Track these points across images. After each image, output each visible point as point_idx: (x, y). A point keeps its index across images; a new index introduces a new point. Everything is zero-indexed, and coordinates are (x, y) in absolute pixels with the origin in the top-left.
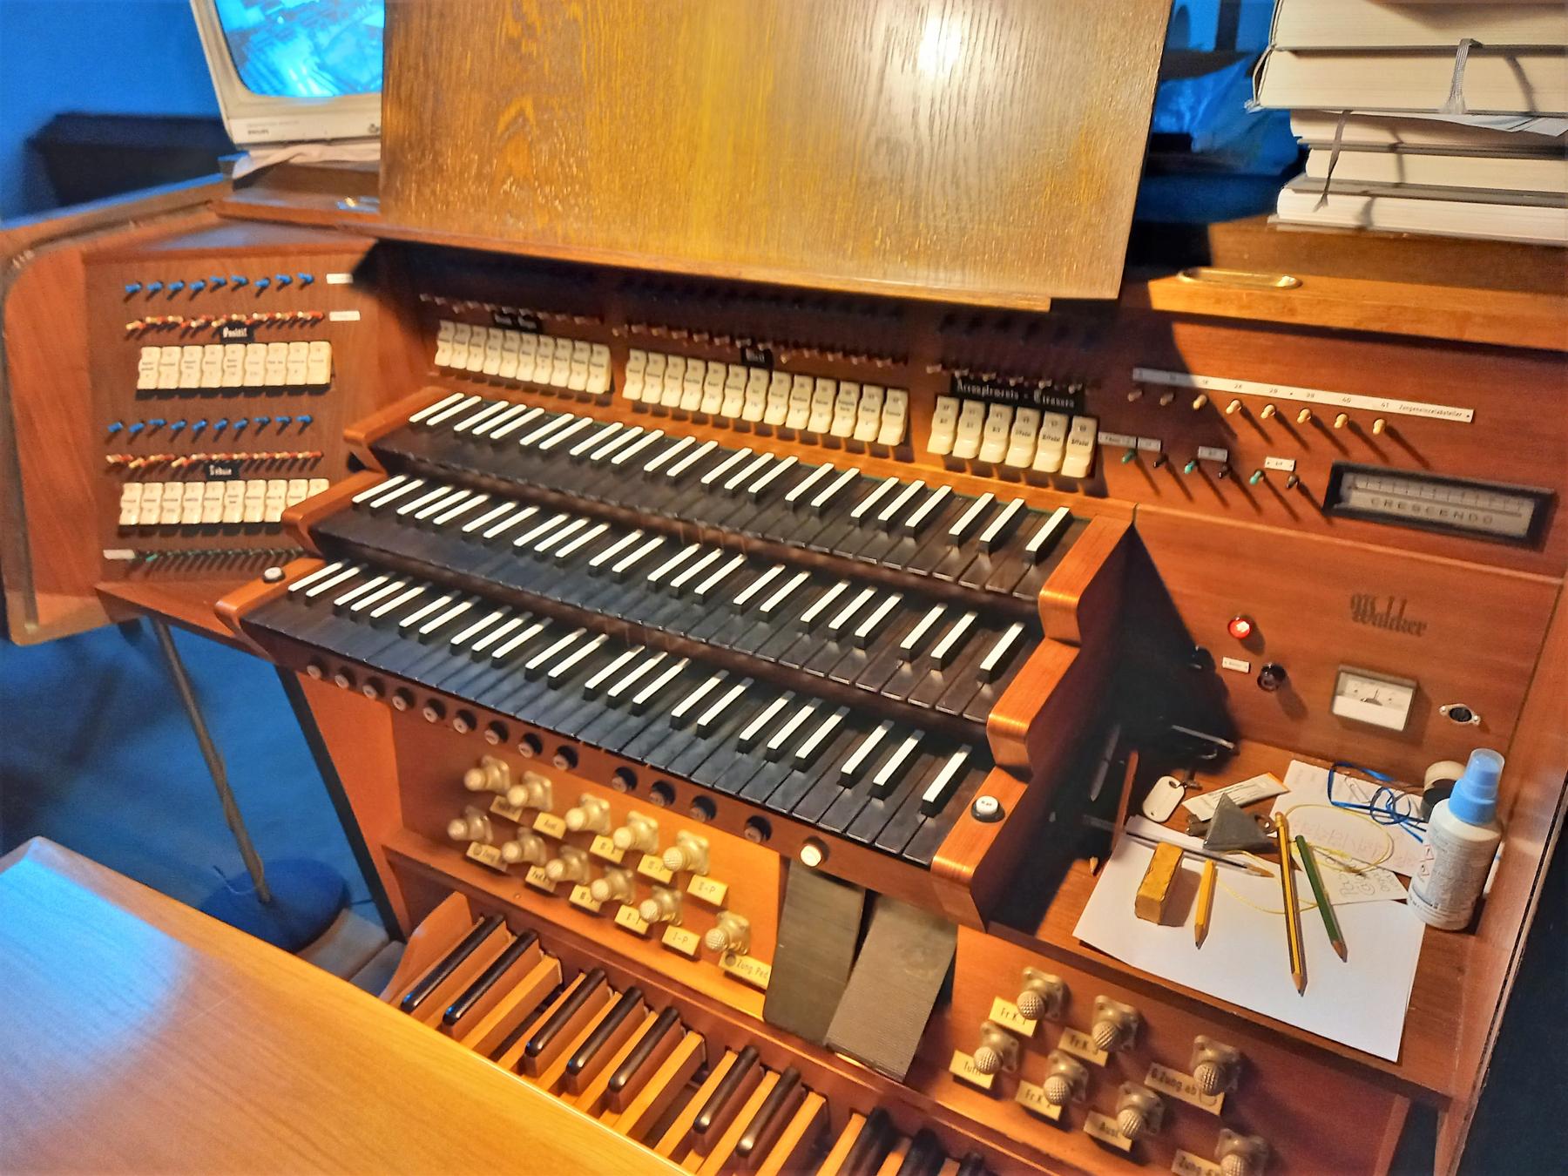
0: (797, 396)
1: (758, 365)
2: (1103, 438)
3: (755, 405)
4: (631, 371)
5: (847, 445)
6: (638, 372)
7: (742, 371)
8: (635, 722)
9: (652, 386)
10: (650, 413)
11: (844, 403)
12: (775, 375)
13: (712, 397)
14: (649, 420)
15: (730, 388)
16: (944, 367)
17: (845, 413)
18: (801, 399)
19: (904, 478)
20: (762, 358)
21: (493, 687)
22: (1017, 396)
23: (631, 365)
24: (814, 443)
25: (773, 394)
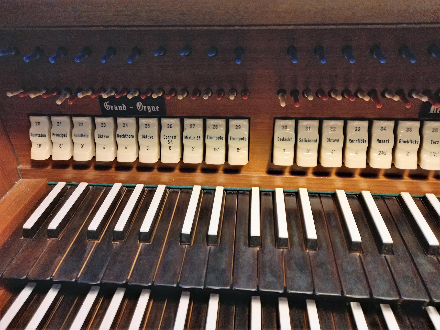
14: (70, 173)
16: (94, 92)
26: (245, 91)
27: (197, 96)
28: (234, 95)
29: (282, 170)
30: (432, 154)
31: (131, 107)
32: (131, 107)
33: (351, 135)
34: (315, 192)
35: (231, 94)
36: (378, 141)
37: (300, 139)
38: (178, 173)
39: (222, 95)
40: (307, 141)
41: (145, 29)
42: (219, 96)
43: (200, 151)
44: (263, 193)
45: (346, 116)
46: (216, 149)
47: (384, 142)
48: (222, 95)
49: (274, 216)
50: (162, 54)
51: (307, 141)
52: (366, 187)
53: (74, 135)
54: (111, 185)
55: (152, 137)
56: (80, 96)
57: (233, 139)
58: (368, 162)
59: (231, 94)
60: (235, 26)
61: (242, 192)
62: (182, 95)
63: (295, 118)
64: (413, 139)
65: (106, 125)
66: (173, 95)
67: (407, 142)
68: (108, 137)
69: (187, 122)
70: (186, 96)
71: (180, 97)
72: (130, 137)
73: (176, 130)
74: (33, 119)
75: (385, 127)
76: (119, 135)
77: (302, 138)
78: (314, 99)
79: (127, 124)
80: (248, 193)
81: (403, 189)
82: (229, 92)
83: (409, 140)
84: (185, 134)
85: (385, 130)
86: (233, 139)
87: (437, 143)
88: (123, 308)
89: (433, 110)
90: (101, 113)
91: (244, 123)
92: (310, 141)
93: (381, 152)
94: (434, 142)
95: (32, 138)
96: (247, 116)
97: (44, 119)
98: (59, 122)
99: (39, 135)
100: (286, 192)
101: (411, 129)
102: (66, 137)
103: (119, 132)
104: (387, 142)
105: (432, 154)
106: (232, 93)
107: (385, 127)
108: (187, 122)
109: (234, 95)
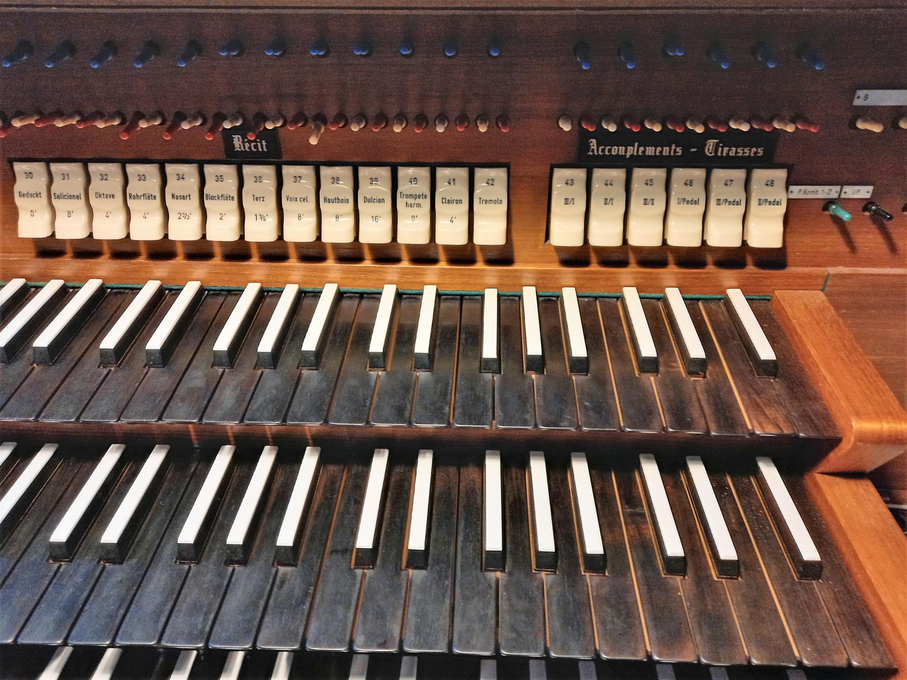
0: (331, 197)
1: (256, 159)
2: (797, 192)
3: (263, 218)
4: (22, 195)
5: (259, 252)
6: (38, 195)
7: (228, 171)
8: (118, 574)
9: (69, 214)
10: (69, 255)
11: (408, 196)
12: (288, 171)
13: (185, 216)
14: (69, 266)
15: (137, 197)
16: (83, 120)
17: (415, 211)
18: (338, 200)
19: (305, 283)
20: (263, 146)
21: (129, 603)
22: (679, 151)
23: (21, 185)
24: (133, 255)
25: (481, 201)
26: (503, 118)
27: (341, 126)
28: (444, 124)
29: (62, 249)
30: (258, 217)
31: (693, 150)
32: (693, 150)
33: (404, 187)
34: (454, 293)
35: (438, 123)
36: (173, 196)
37: (54, 194)
38: (257, 263)
39: (466, 125)
40: (66, 197)
41: (386, 12)
42: (377, 124)
43: (158, 218)
44: (541, 299)
45: (356, 160)
46: (375, 218)
47: (184, 198)
48: (466, 125)
49: (100, 332)
50: (235, 54)
51: (375, 201)
52: (572, 283)
53: (325, 200)
54: (139, 286)
55: (113, 196)
56: (17, 124)
57: (484, 202)
58: (745, 239)
59: (438, 123)
60: (574, 9)
61: (408, 296)
62: (359, 124)
63: (352, 162)
64: (226, 192)
65: (146, 178)
66: (300, 125)
67: (217, 198)
68: (113, 196)
69: (364, 172)
70: (364, 127)
71: (397, 129)
72: (342, 201)
73: (346, 187)
74: (19, 167)
75: (612, 181)
76: (328, 198)
77: (58, 193)
78: (882, 132)
79: (183, 175)
80: (517, 298)
81: (627, 283)
82: (435, 120)
83: (220, 195)
84: (129, 190)
85: (183, 179)
86: (484, 202)
87: (261, 199)
88: (665, 570)
89: (239, 147)
90: (223, 157)
91: (500, 174)
92: (71, 197)
93: (182, 215)
94: (257, 199)
95: (19, 201)
96: (389, 161)
97: (38, 168)
98: (258, 176)
99: (105, 196)
100: (541, 296)
101: (691, 181)
102: (780, 206)
103: (56, 188)
104: (188, 197)
105: (258, 217)
106: (484, 121)
107: (612, 181)
108: (364, 172)
109: (402, 125)
